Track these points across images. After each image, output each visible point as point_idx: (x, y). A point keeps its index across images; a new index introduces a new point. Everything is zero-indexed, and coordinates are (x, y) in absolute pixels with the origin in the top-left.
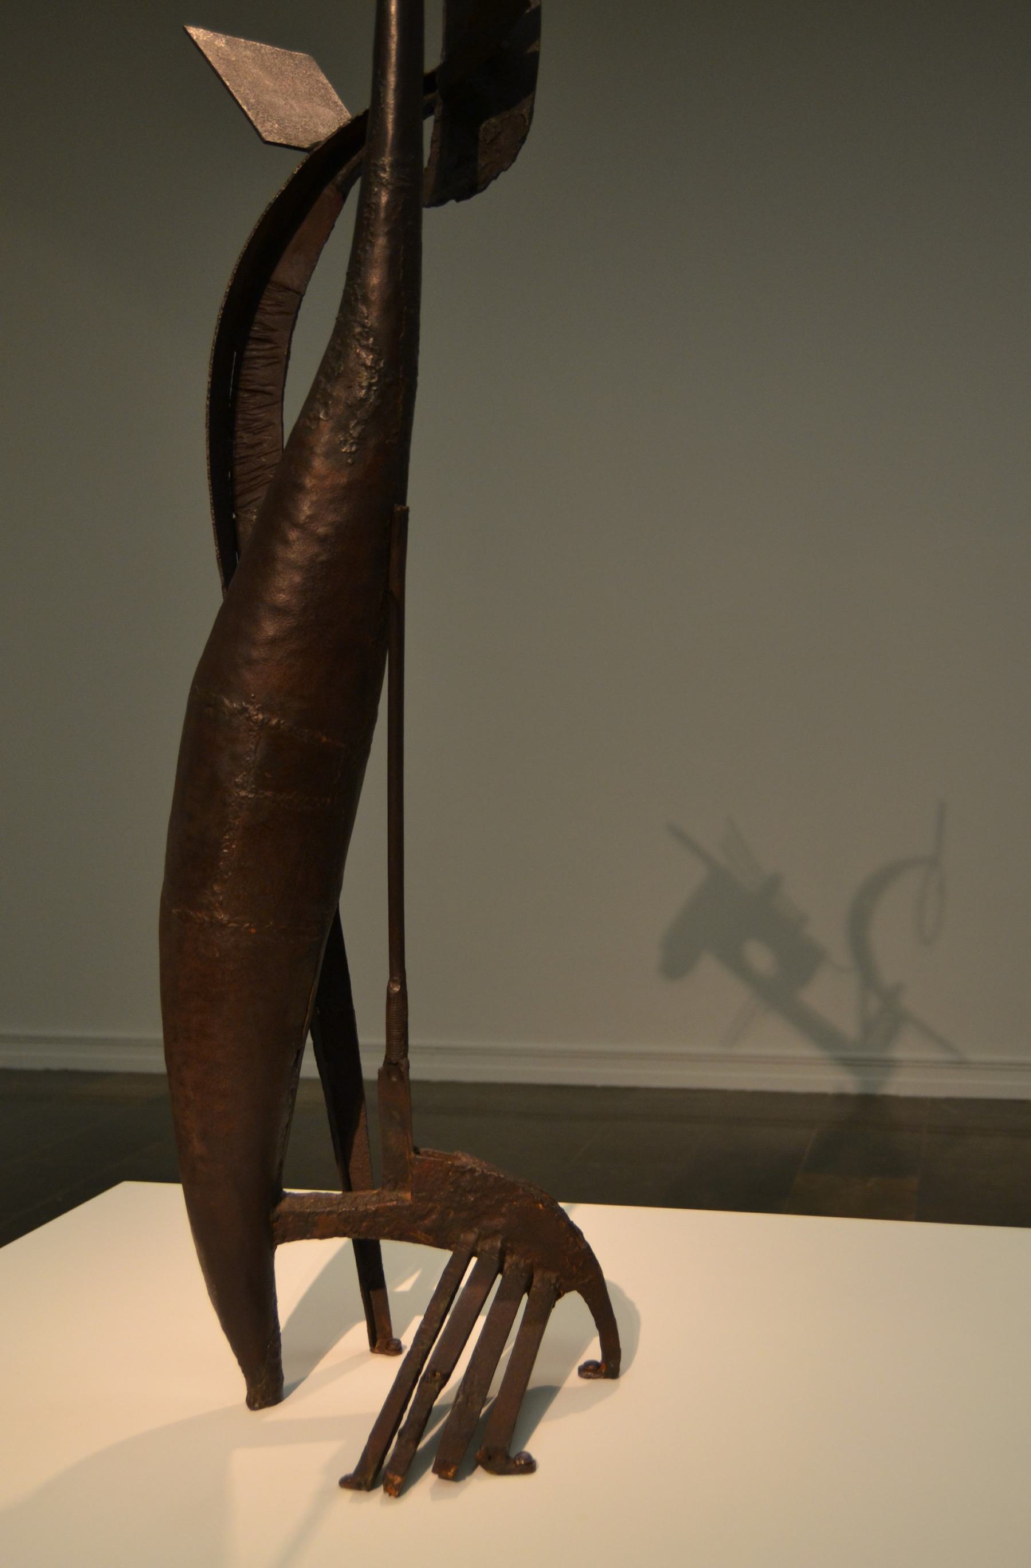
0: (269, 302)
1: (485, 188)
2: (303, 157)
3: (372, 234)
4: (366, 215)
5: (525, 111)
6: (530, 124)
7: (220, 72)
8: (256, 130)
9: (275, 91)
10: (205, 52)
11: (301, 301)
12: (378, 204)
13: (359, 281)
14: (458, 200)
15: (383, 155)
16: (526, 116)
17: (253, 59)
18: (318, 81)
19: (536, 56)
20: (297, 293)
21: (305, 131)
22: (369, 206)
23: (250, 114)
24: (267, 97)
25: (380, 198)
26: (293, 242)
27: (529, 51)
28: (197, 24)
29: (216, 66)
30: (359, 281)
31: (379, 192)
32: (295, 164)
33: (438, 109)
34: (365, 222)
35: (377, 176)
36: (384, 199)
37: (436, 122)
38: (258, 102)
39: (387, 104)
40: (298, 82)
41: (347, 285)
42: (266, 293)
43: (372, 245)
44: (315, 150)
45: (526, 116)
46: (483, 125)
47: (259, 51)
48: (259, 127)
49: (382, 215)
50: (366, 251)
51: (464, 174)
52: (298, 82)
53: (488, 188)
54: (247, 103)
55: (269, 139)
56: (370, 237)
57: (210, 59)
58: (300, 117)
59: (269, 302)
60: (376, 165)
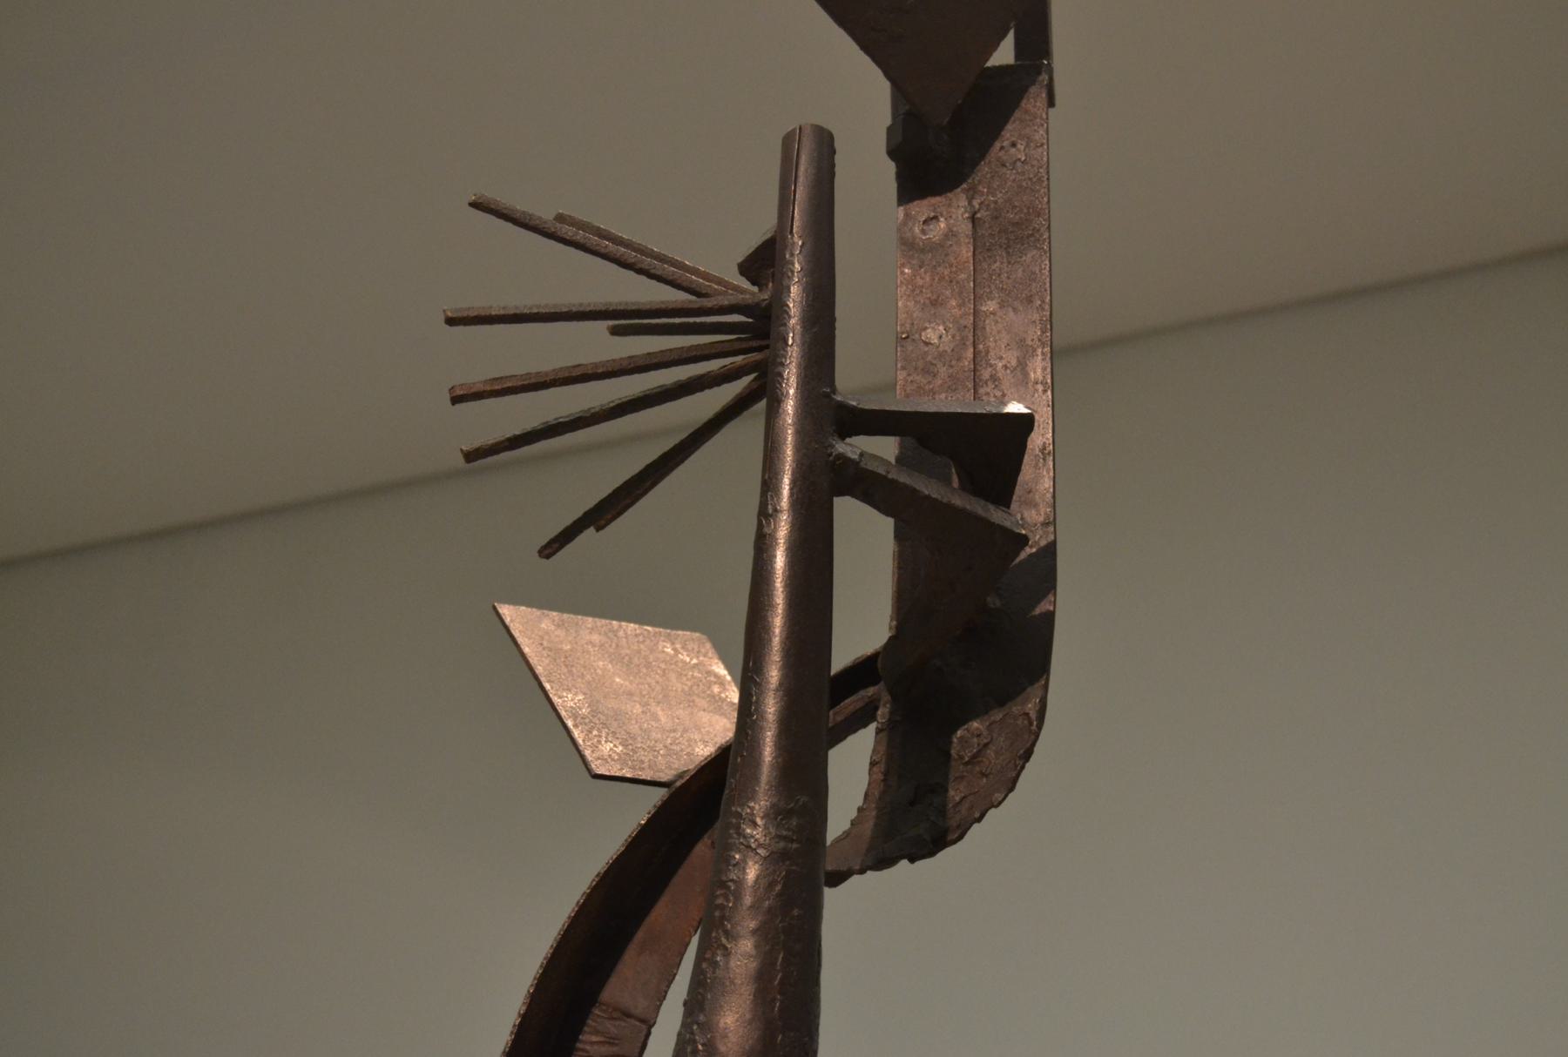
0: (594, 1039)
1: (960, 838)
2: (659, 795)
3: (727, 933)
4: (720, 901)
5: (1031, 707)
6: (1040, 727)
7: (539, 670)
8: (583, 757)
9: (630, 694)
10: (520, 640)
11: (648, 1034)
12: (740, 883)
13: (702, 1018)
14: (912, 860)
15: (752, 798)
16: (1033, 715)
17: (602, 645)
18: (709, 673)
19: (1049, 617)
20: (643, 1021)
21: (670, 752)
22: (723, 885)
23: (576, 733)
24: (612, 704)
25: (744, 873)
26: (640, 935)
27: (1037, 611)
28: (514, 601)
29: (533, 661)
30: (702, 1018)
31: (744, 861)
32: (640, 809)
33: (883, 712)
34: (717, 914)
35: (740, 834)
36: (752, 873)
37: (878, 731)
38: (595, 712)
39: (762, 717)
40: (673, 676)
41: (684, 1025)
42: (589, 1022)
43: (727, 953)
44: (678, 784)
45: (1033, 715)
46: (959, 733)
47: (615, 633)
48: (587, 753)
49: (748, 900)
50: (715, 964)
51: (916, 819)
52: (673, 676)
53: (967, 837)
54: (575, 716)
55: (599, 772)
56: (724, 940)
57: (526, 650)
58: (663, 730)
59: (594, 1039)
60: (739, 816)
